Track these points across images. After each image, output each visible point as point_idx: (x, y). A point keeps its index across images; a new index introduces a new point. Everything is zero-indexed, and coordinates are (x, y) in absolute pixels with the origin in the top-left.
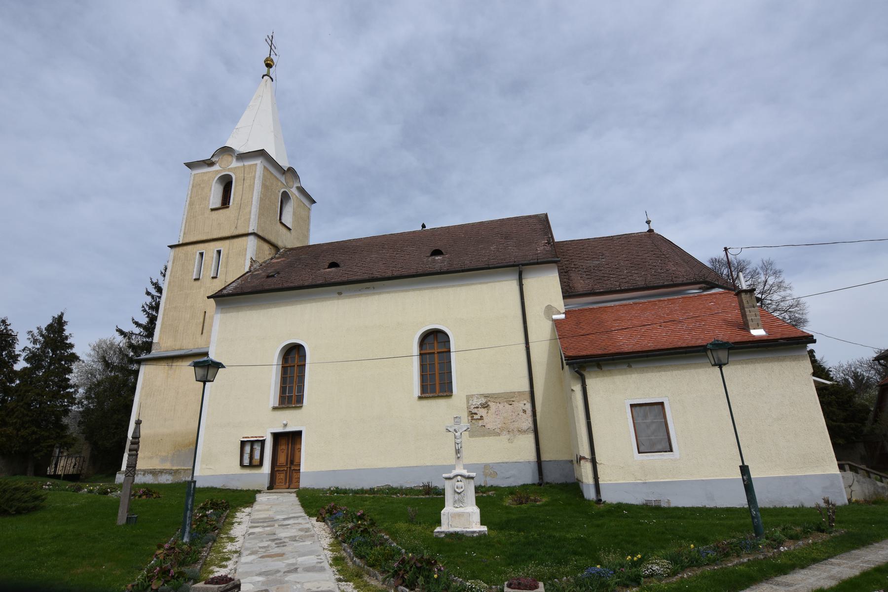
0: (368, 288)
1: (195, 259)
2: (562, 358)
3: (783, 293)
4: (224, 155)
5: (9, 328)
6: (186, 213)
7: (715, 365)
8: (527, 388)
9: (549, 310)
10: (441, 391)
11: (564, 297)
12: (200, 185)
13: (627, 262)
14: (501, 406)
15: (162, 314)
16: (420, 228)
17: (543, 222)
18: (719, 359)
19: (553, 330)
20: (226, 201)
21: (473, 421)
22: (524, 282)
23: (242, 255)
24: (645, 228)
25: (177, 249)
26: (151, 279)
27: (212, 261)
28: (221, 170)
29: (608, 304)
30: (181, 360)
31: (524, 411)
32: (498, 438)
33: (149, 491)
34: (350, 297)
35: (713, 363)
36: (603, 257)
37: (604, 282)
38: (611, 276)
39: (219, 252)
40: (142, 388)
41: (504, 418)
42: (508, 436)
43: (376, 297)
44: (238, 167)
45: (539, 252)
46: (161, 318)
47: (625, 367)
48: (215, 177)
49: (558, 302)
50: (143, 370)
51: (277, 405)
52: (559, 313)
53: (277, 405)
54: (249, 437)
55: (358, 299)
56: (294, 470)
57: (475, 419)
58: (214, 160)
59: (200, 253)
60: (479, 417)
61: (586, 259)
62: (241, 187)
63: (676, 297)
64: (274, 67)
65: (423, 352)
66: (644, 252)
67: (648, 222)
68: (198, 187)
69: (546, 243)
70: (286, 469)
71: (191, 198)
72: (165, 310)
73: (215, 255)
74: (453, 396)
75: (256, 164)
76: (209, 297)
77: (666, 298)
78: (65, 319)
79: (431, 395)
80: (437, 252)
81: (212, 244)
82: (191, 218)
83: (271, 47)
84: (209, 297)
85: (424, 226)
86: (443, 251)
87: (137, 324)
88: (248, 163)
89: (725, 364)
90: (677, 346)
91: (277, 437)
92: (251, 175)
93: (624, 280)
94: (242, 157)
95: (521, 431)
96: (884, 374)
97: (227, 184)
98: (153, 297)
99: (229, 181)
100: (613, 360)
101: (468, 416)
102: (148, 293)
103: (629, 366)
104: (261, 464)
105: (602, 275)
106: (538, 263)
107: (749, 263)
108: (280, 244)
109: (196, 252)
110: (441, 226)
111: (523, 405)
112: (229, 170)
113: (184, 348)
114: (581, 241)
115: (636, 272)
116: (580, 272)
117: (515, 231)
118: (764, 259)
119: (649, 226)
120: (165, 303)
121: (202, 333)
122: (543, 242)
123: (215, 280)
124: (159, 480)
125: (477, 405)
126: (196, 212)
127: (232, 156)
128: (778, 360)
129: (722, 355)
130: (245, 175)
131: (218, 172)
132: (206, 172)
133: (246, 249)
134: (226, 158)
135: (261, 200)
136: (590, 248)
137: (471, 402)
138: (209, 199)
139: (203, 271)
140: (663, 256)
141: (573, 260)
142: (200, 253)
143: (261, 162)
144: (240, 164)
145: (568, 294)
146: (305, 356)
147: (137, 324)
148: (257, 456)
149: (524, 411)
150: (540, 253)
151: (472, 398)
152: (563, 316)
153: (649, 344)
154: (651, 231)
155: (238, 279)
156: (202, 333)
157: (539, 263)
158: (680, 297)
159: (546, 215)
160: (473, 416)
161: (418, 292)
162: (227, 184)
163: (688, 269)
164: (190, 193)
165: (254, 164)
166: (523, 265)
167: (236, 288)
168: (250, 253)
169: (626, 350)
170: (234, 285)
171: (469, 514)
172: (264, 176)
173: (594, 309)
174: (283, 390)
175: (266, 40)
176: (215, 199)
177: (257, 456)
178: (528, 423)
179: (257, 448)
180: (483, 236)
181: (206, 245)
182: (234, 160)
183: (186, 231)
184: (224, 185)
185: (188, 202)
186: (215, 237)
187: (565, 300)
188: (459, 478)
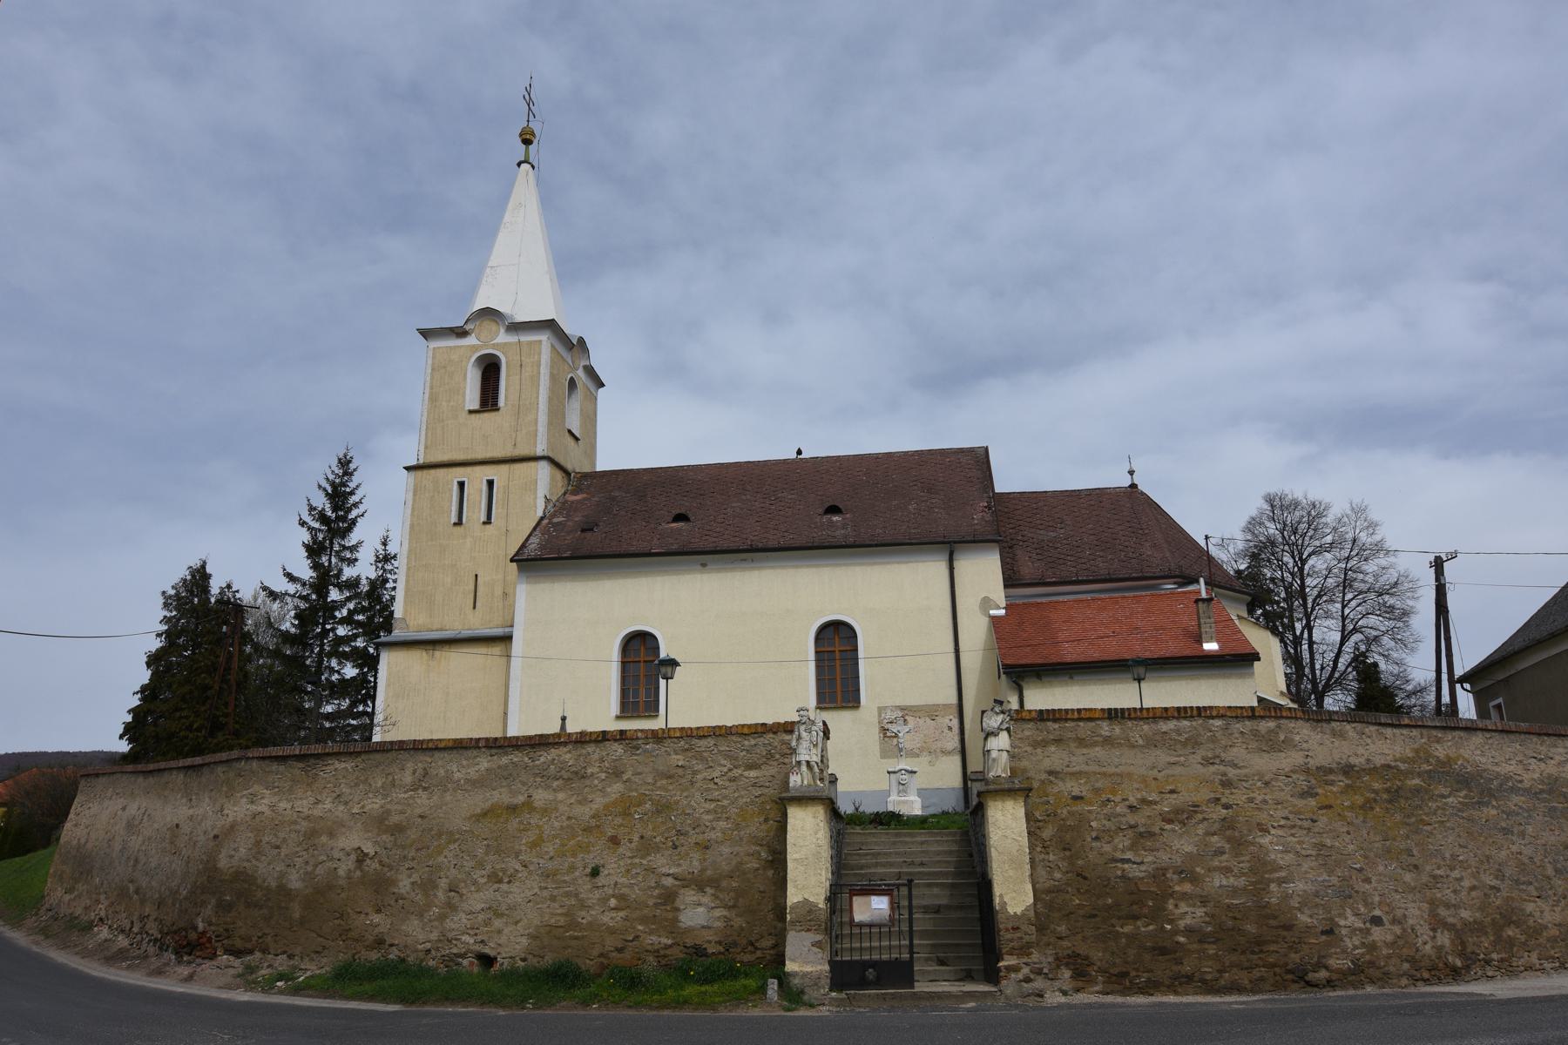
0: (745, 560)
1: (451, 490)
2: (999, 670)
3: (1383, 562)
4: (483, 321)
5: (238, 596)
6: (425, 414)
7: (1135, 680)
8: (954, 700)
9: (986, 603)
10: (843, 701)
11: (1006, 586)
12: (445, 367)
13: (1091, 537)
14: (921, 721)
15: (404, 574)
16: (794, 456)
17: (979, 461)
18: (1138, 675)
19: (989, 630)
20: (489, 399)
21: (886, 739)
22: (956, 564)
23: (530, 490)
24: (1126, 482)
25: (419, 473)
26: (309, 500)
27: (481, 496)
29: (1061, 598)
30: (448, 647)
31: (950, 728)
33: (617, 776)
34: (719, 571)
35: (1136, 677)
36: (1063, 525)
37: (1059, 567)
38: (1069, 558)
39: (490, 483)
40: (388, 685)
41: (925, 736)
42: (929, 758)
43: (756, 573)
44: (510, 344)
45: (976, 522)
47: (1067, 678)
48: (471, 357)
49: (998, 594)
50: (386, 661)
51: (618, 713)
52: (998, 608)
55: (729, 575)
58: (467, 327)
59: (459, 482)
61: (1040, 527)
62: (518, 377)
63: (1144, 593)
64: (535, 142)
65: (818, 650)
66: (1117, 522)
67: (1131, 473)
68: (439, 368)
69: (986, 507)
71: (431, 388)
73: (485, 487)
74: (861, 708)
75: (540, 341)
77: (1132, 594)
78: (209, 570)
79: (832, 705)
80: (833, 510)
81: (478, 469)
82: (435, 425)
83: (529, 105)
85: (799, 452)
86: (841, 507)
87: (291, 578)
88: (527, 338)
89: (1143, 679)
90: (1121, 658)
92: (532, 360)
93: (1084, 566)
94: (516, 327)
95: (945, 752)
97: (490, 370)
98: (310, 529)
100: (1054, 670)
101: (880, 733)
102: (303, 523)
103: (1071, 678)
105: (1057, 555)
106: (974, 542)
107: (1327, 508)
108: (569, 467)
110: (827, 455)
111: (948, 721)
112: (495, 346)
113: (447, 628)
114: (1035, 495)
115: (1101, 554)
116: (1029, 549)
117: (941, 479)
118: (1354, 501)
119: (1132, 478)
120: (408, 557)
121: (474, 607)
122: (981, 505)
123: (488, 526)
126: (1251, 800)
127: (498, 324)
128: (1224, 676)
129: (1141, 670)
130: (523, 358)
131: (474, 348)
132: (455, 347)
134: (488, 325)
136: (1045, 508)
137: (883, 715)
138: (464, 393)
139: (467, 512)
140: (1141, 532)
141: (1022, 528)
142: (459, 482)
143: (548, 338)
144: (512, 339)
145: (1010, 581)
146: (658, 648)
147: (291, 578)
149: (950, 728)
150: (977, 524)
152: (1003, 612)
153: (1096, 655)
154: (1133, 486)
155: (535, 529)
156: (474, 607)
157: (976, 541)
158: (1149, 593)
159: (986, 449)
161: (814, 570)
162: (490, 370)
163: (1168, 554)
164: (428, 379)
165: (536, 341)
166: (955, 542)
168: (543, 489)
169: (1069, 660)
170: (535, 540)
171: (912, 802)
172: (552, 360)
173: (1042, 603)
174: (624, 693)
175: (524, 97)
176: (471, 394)
178: (953, 742)
180: (896, 484)
181: (469, 469)
182: (502, 330)
183: (429, 443)
184: (483, 366)
185: (427, 396)
186: (480, 456)
187: (1007, 590)
188: (903, 772)
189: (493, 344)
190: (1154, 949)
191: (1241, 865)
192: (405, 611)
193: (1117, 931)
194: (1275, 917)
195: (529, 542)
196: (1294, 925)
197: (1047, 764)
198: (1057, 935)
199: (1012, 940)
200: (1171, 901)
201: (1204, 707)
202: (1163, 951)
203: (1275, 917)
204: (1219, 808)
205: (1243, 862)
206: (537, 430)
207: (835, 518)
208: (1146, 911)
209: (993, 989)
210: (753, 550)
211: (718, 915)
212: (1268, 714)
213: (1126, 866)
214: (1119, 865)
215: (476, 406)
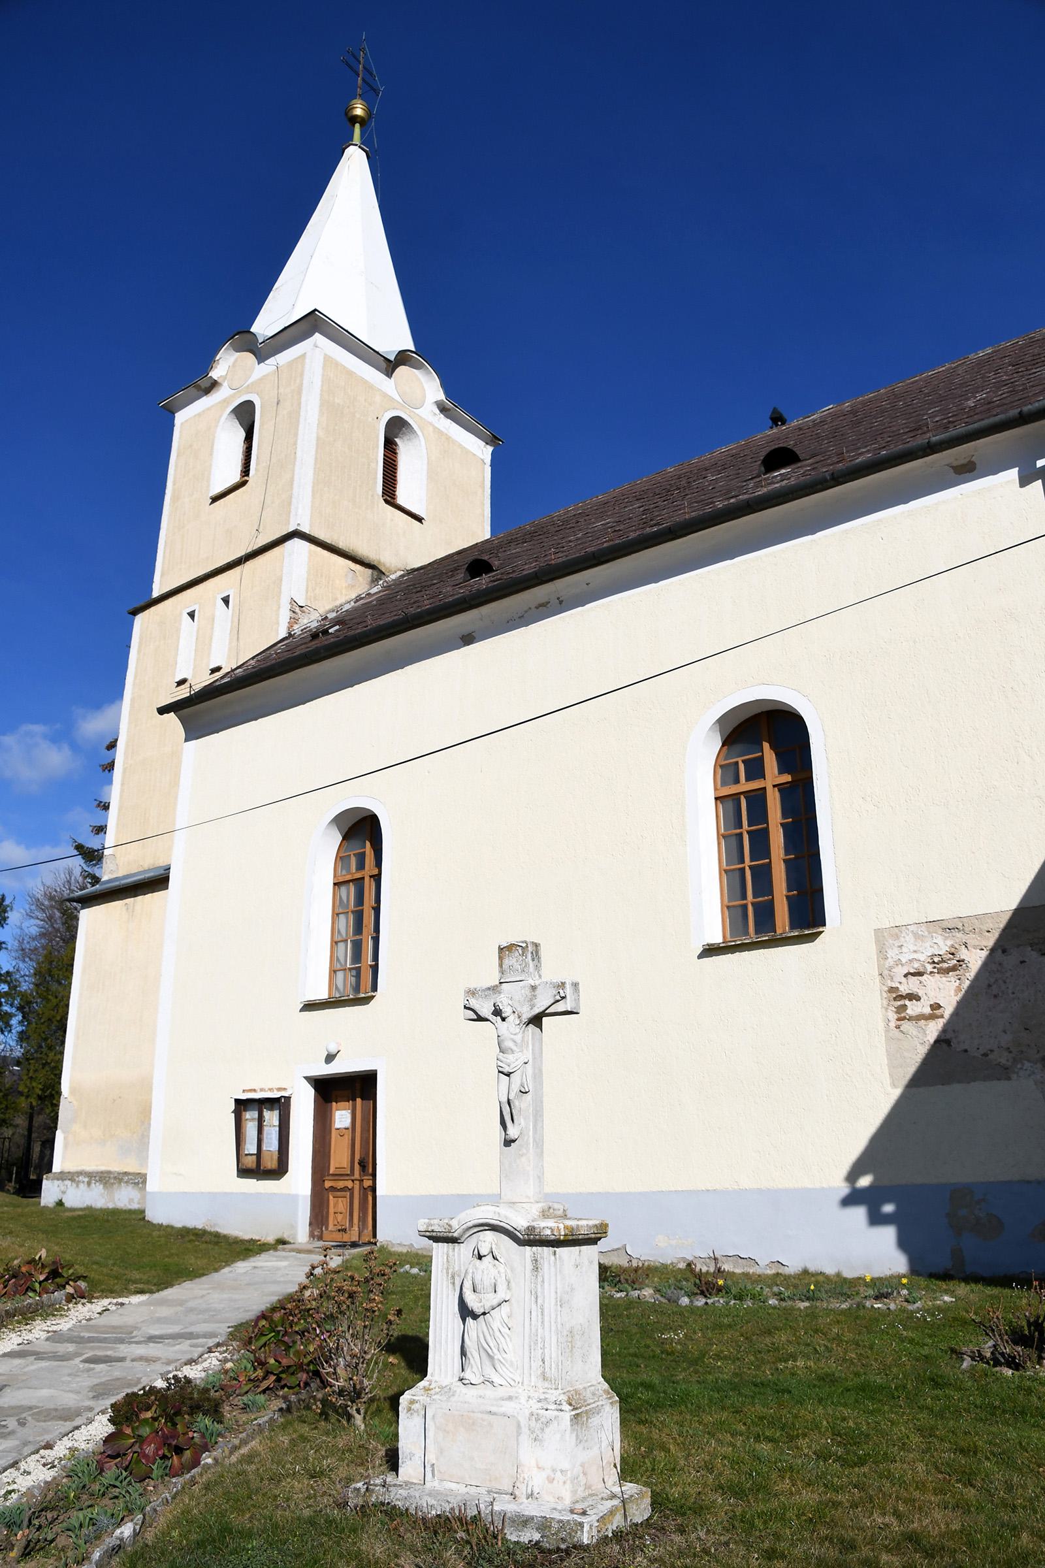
12: (191, 446)
21: (906, 1026)
28: (233, 396)
32: (1002, 1086)
46: (119, 791)
48: (220, 417)
54: (255, 1090)
56: (333, 1189)
57: (910, 1019)
60: (927, 1010)
70: (349, 1184)
72: (125, 770)
75: (304, 355)
76: (162, 711)
84: (162, 711)
104: (280, 1170)
109: (181, 614)
112: (249, 389)
124: (116, 1199)
125: (916, 965)
131: (226, 401)
135: (320, 444)
137: (892, 954)
151: (897, 937)
155: (253, 658)
160: (905, 1007)
179: (272, 1117)
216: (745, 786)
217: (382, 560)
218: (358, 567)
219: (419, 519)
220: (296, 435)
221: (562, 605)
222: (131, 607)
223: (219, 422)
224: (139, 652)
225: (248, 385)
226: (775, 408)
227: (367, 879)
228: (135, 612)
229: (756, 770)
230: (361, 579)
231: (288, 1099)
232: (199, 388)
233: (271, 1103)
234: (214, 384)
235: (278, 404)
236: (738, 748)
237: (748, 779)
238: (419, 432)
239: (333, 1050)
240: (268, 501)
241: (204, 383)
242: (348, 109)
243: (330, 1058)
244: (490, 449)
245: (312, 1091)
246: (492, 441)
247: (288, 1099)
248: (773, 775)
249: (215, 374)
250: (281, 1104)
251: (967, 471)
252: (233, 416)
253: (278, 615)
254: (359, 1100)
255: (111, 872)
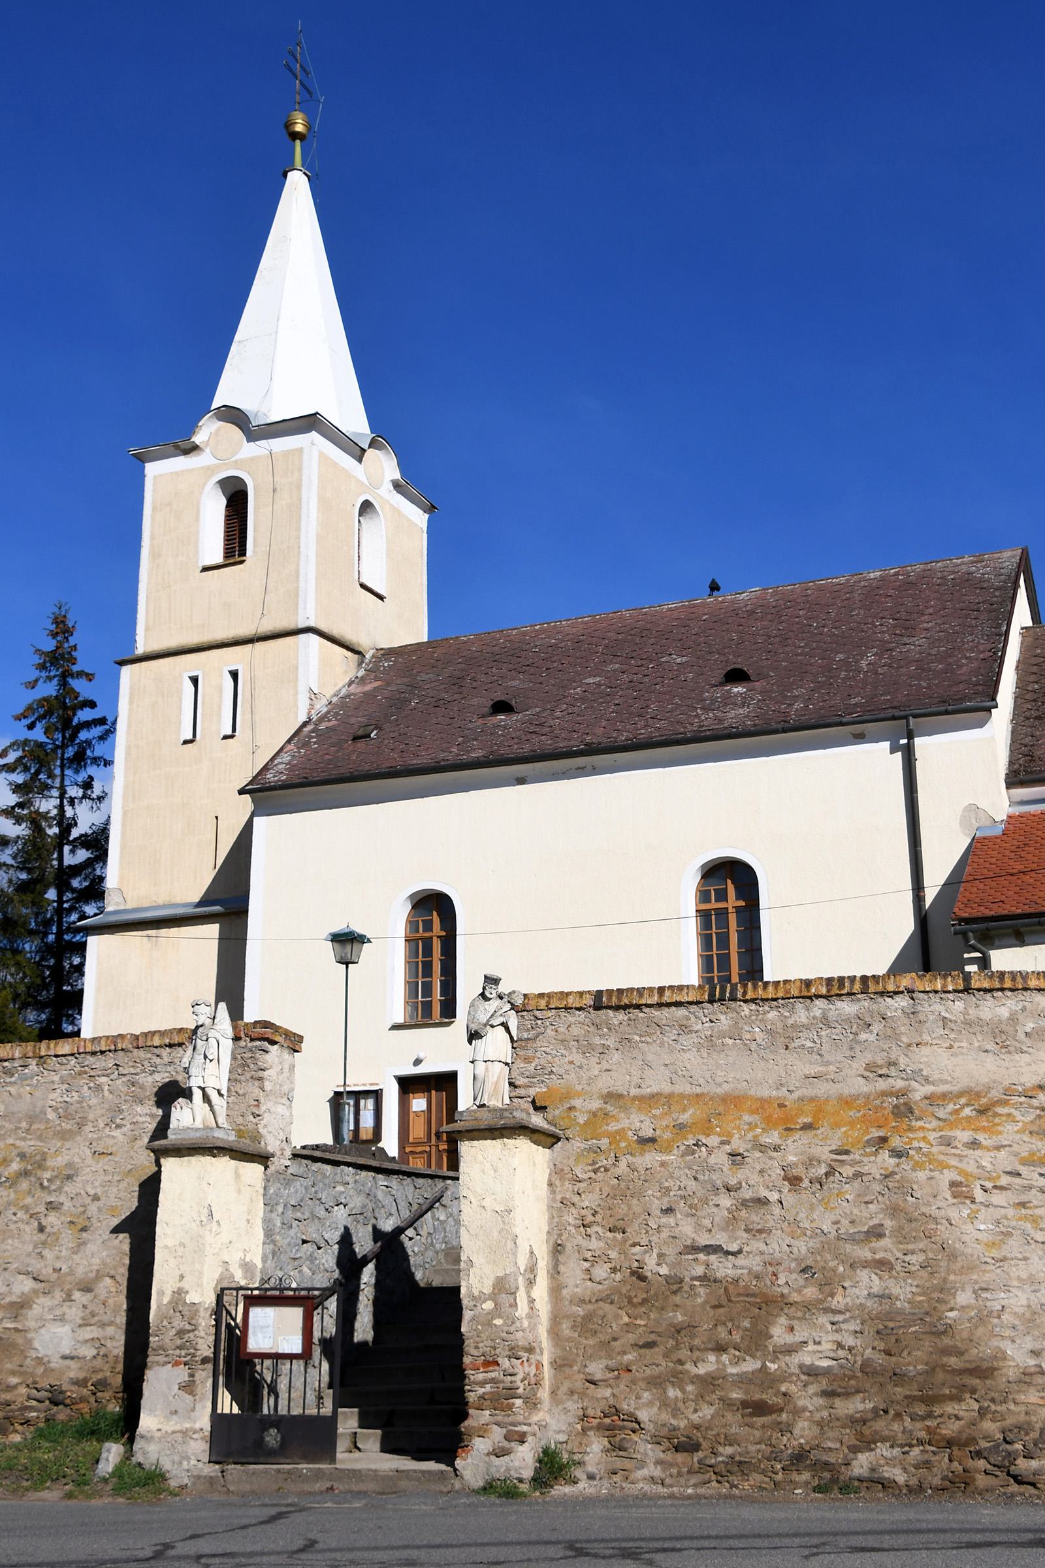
12: (170, 504)
48: (205, 484)
53: (400, 1020)
56: (412, 1152)
59: (230, 672)
70: (427, 1149)
75: (301, 450)
80: (736, 676)
91: (408, 1085)
96: (55, 904)
99: (238, 488)
109: (181, 676)
112: (237, 464)
131: (209, 470)
133: (297, 669)
135: (320, 539)
148: (367, 1120)
155: (289, 741)
167: (291, 767)
170: (286, 757)
177: (367, 1120)
179: (368, 1105)
187: (1013, 791)
189: (236, 461)
190: (745, 1404)
191: (907, 1258)
192: (122, 878)
193: (687, 1371)
194: (960, 1353)
195: (276, 762)
196: (996, 1369)
197: (605, 1083)
198: (589, 1378)
199: (482, 1384)
200: (783, 1320)
201: (874, 976)
202: (759, 1408)
203: (960, 1353)
204: (885, 1155)
205: (913, 1252)
206: (297, 589)
207: (738, 689)
208: (737, 1337)
209: (442, 1467)
210: (592, 750)
211: (88, 1336)
212: (998, 986)
213: (713, 1258)
214: (701, 1256)
215: (218, 558)
216: (714, 905)
217: (361, 642)
218: (349, 654)
219: (381, 597)
220: (298, 529)
221: (595, 771)
222: (119, 658)
223: (203, 489)
224: (131, 703)
225: (236, 461)
226: (713, 580)
227: (435, 939)
228: (122, 663)
229: (722, 896)
230: (351, 664)
231: (382, 1090)
232: (177, 447)
233: (366, 1094)
234: (195, 448)
235: (274, 491)
236: (711, 880)
237: (716, 901)
238: (380, 513)
239: (422, 1056)
240: (271, 586)
241: (184, 445)
242: (288, 125)
243: (417, 1062)
244: (427, 516)
245: (397, 1086)
246: (430, 509)
247: (382, 1090)
248: (733, 901)
249: (198, 439)
250: (377, 1095)
251: (860, 738)
252: (218, 485)
253: (296, 699)
254: (433, 1092)
255: (117, 904)
